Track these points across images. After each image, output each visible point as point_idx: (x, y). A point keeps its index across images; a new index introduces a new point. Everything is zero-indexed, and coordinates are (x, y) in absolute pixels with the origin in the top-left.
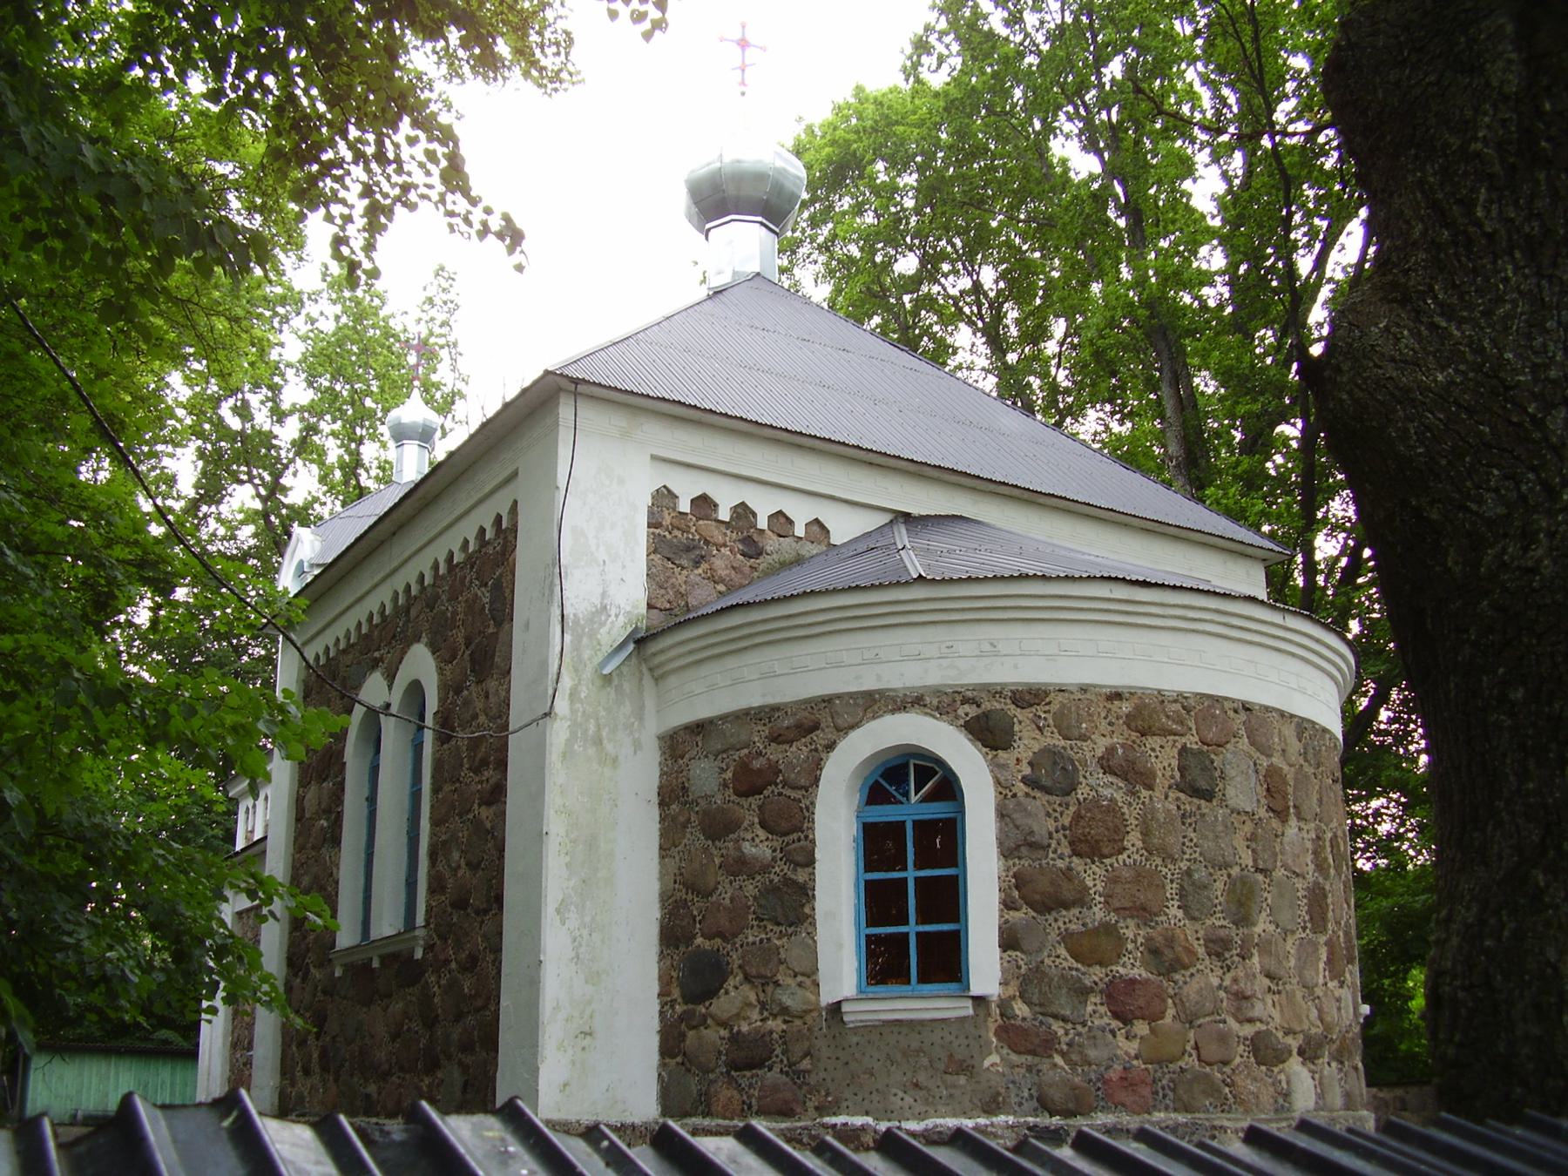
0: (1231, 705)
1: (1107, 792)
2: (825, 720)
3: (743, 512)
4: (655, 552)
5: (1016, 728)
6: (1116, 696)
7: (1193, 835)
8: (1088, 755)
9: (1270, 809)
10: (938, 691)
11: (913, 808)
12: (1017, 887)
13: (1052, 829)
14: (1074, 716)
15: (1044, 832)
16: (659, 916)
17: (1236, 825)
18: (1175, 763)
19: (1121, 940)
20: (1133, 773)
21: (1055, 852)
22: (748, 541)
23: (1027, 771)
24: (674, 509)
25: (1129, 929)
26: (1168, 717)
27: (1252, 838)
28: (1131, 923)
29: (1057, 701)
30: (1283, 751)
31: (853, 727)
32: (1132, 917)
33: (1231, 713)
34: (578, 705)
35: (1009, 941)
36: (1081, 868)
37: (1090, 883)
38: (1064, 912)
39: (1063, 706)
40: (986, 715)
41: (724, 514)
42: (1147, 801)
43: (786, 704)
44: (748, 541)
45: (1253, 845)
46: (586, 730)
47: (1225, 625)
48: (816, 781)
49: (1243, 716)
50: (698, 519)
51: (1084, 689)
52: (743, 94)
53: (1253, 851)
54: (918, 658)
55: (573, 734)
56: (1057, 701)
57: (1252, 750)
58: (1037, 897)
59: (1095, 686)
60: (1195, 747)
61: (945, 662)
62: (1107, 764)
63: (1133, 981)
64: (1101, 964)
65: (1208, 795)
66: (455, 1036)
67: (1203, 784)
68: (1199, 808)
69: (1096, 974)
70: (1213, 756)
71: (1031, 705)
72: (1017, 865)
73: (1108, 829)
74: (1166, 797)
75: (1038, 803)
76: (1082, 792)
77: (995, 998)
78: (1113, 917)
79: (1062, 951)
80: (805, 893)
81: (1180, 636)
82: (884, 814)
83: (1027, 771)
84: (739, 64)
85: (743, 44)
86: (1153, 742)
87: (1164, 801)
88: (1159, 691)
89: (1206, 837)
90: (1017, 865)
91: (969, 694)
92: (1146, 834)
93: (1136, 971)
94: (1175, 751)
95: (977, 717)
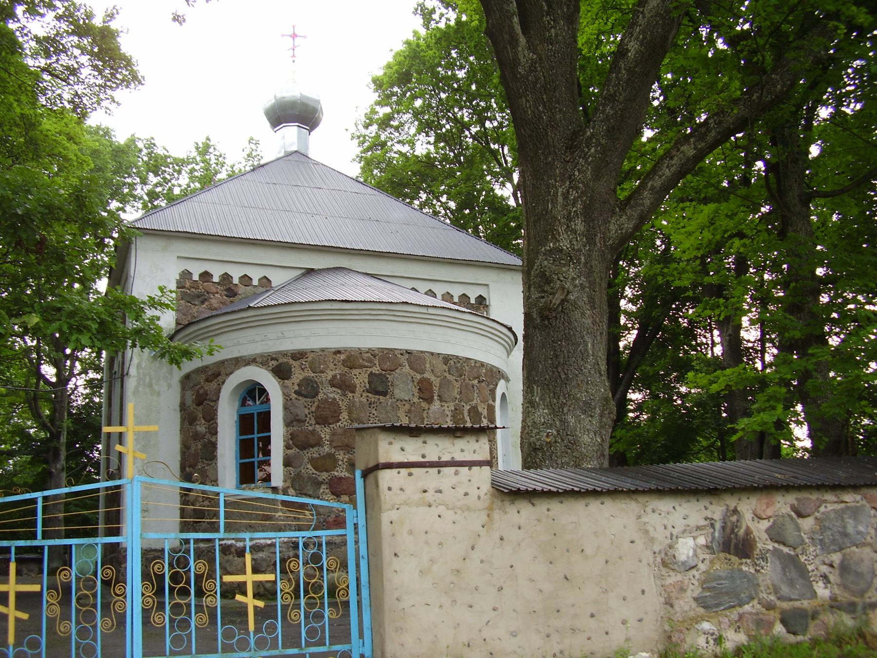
0: (399, 352)
1: (332, 396)
2: (223, 371)
3: (226, 277)
4: (182, 299)
5: (293, 370)
6: (338, 352)
7: (374, 412)
8: (324, 379)
9: (420, 398)
10: (262, 356)
11: (254, 408)
12: (291, 439)
13: (307, 413)
14: (317, 362)
15: (303, 415)
16: (179, 459)
17: (400, 406)
18: (366, 380)
19: (336, 461)
20: (344, 385)
21: (308, 423)
22: (229, 290)
23: (297, 388)
24: (191, 279)
25: (341, 456)
26: (364, 360)
27: (410, 411)
28: (341, 452)
29: (311, 356)
30: (432, 370)
31: (231, 373)
32: (342, 450)
33: (399, 356)
34: (141, 371)
35: (287, 463)
36: (319, 430)
37: (323, 436)
38: (311, 449)
39: (313, 358)
40: (280, 365)
41: (216, 279)
42: (351, 398)
43: (210, 365)
44: (229, 290)
45: (409, 415)
46: (145, 381)
47: (394, 315)
48: (218, 399)
49: (407, 356)
50: (203, 282)
51: (323, 350)
52: (294, 61)
53: (409, 418)
54: (254, 342)
55: (139, 383)
56: (311, 356)
57: (412, 373)
58: (299, 443)
59: (327, 348)
60: (377, 372)
61: (263, 343)
62: (333, 383)
63: (341, 478)
64: (327, 471)
65: (384, 394)
66: (818, 563)
67: (380, 389)
68: (379, 399)
69: (324, 476)
70: (388, 376)
71: (299, 359)
72: (291, 430)
73: (331, 412)
74: (361, 396)
75: (301, 402)
76: (321, 396)
77: (281, 488)
78: (333, 450)
79: (310, 466)
80: (213, 446)
81: (370, 323)
82: (246, 410)
83: (297, 388)
84: (292, 46)
85: (294, 36)
86: (356, 371)
87: (360, 397)
88: (359, 348)
89: (381, 413)
90: (291, 430)
91: (274, 356)
92: (350, 413)
93: (343, 473)
94: (367, 375)
95: (276, 366)
